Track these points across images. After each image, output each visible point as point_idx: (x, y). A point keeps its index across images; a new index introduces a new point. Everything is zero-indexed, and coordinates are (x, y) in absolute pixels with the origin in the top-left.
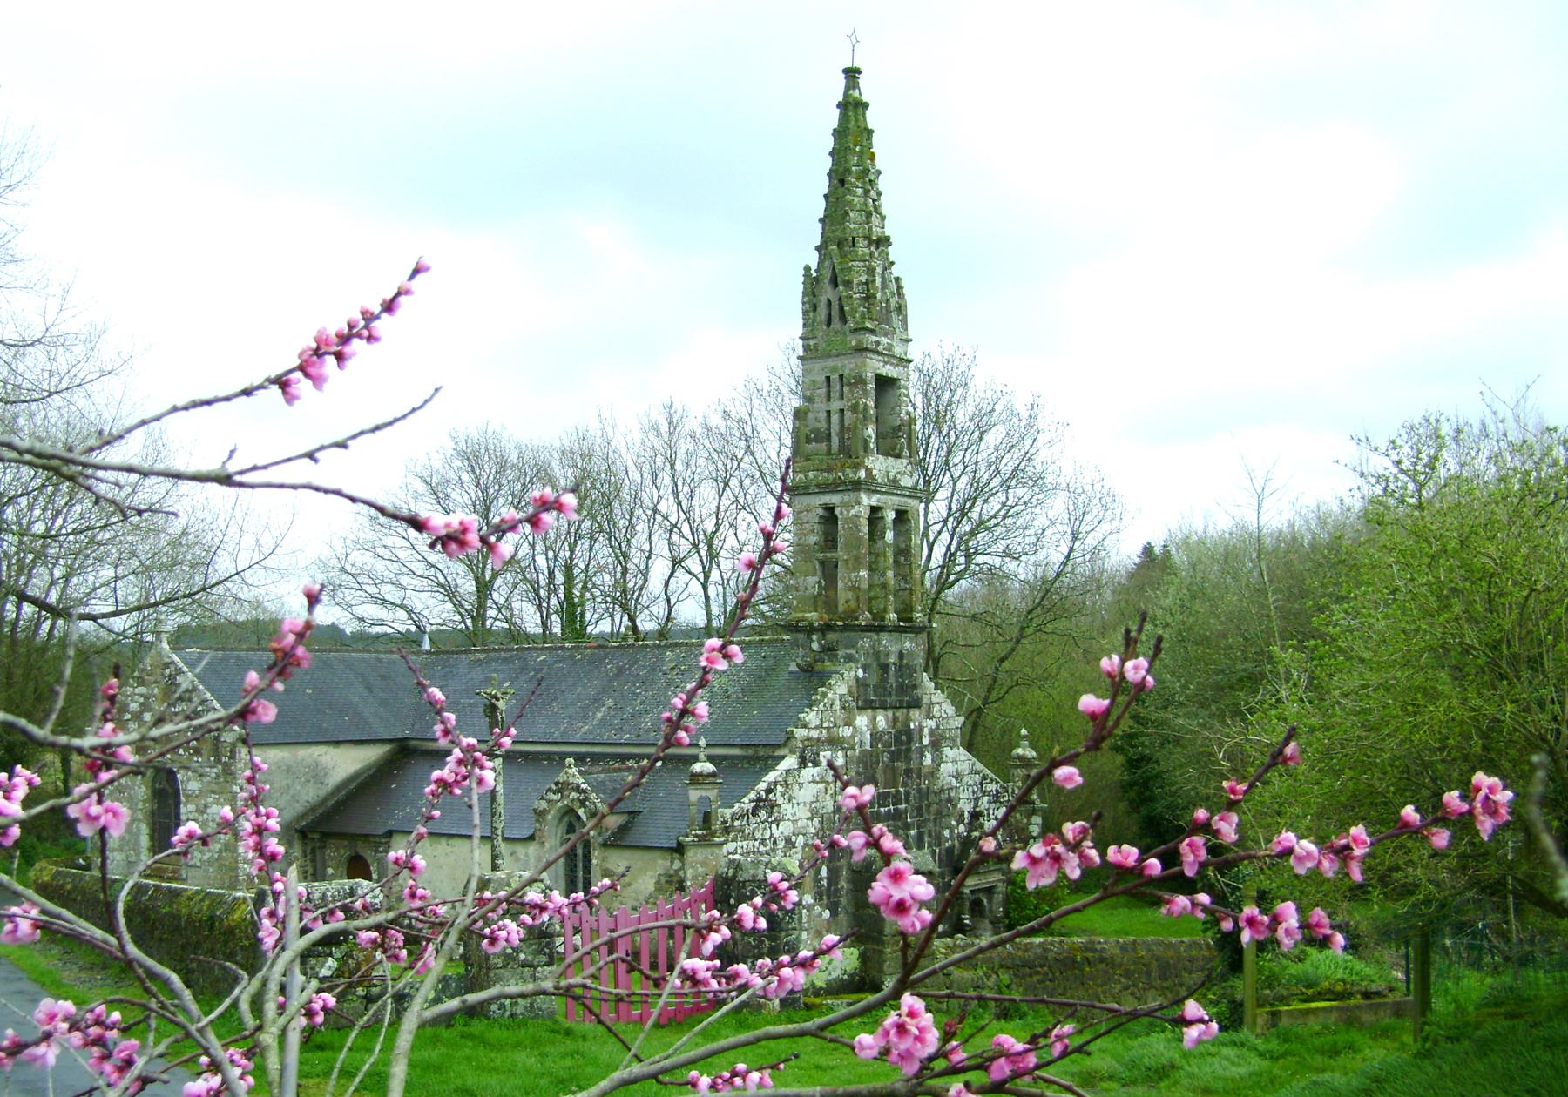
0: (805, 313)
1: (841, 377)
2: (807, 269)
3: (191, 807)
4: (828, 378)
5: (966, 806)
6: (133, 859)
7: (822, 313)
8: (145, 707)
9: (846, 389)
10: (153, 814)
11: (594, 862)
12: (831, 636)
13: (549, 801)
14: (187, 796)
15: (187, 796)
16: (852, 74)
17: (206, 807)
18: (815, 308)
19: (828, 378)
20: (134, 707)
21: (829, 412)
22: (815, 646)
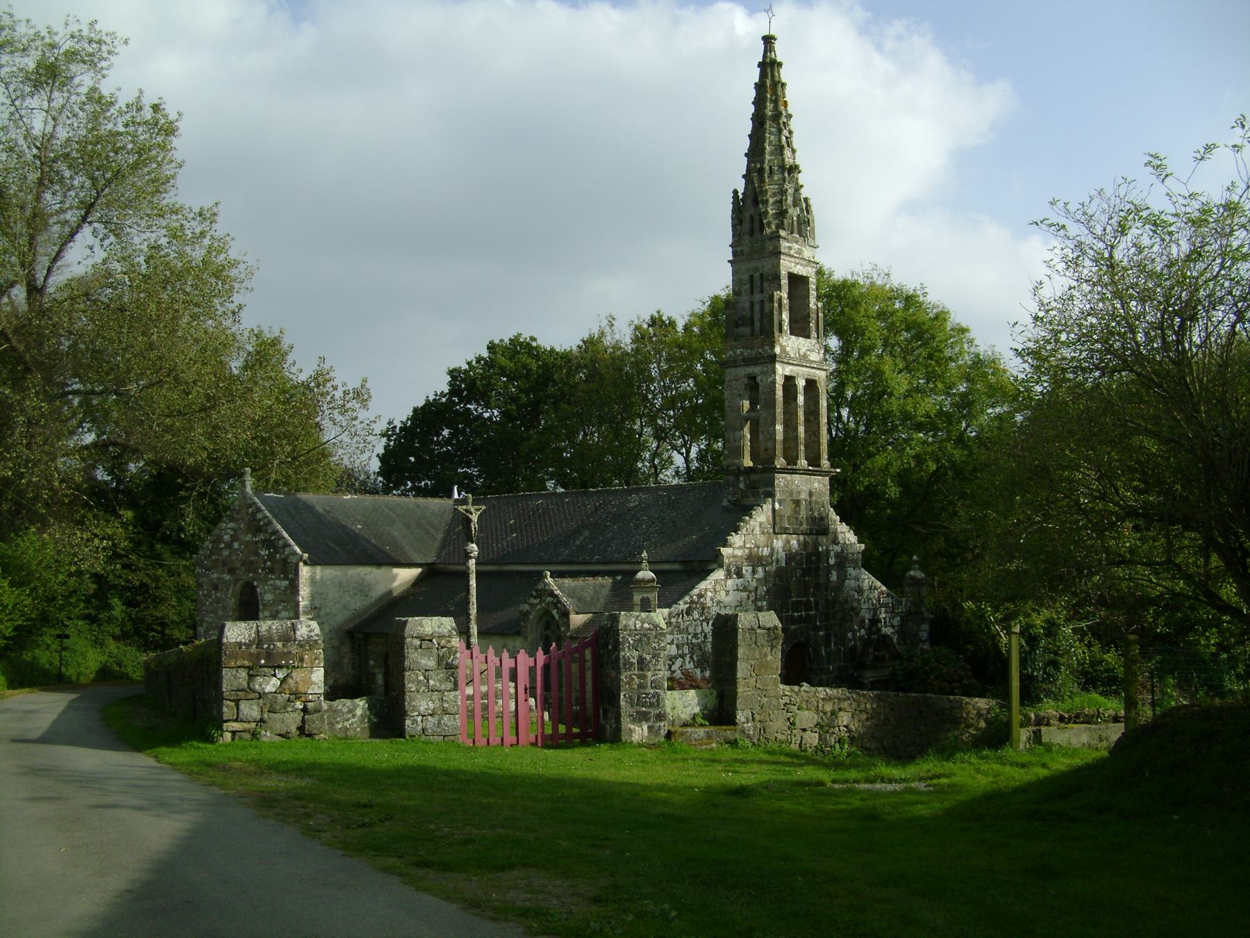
1: (761, 275)
2: (735, 192)
7: (747, 226)
8: (234, 538)
9: (765, 284)
12: (754, 477)
14: (264, 605)
15: (264, 605)
19: (751, 277)
20: (227, 538)
22: (742, 485)
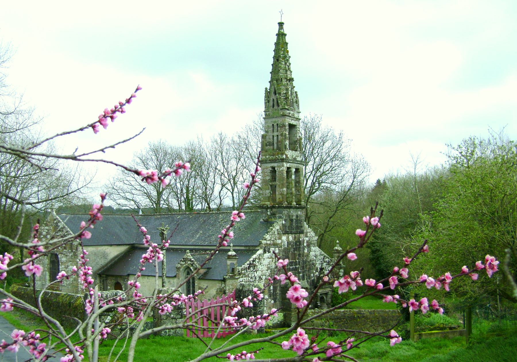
0: (265, 103)
1: (277, 124)
2: (266, 89)
3: (63, 266)
4: (273, 125)
5: (318, 266)
6: (44, 283)
7: (271, 103)
8: (48, 233)
9: (279, 128)
10: (50, 269)
11: (196, 284)
13: (181, 264)
14: (62, 263)
15: (62, 263)
16: (281, 24)
17: (68, 266)
18: (269, 102)
19: (273, 125)
20: (44, 233)
21: (273, 136)
22: (269, 213)
